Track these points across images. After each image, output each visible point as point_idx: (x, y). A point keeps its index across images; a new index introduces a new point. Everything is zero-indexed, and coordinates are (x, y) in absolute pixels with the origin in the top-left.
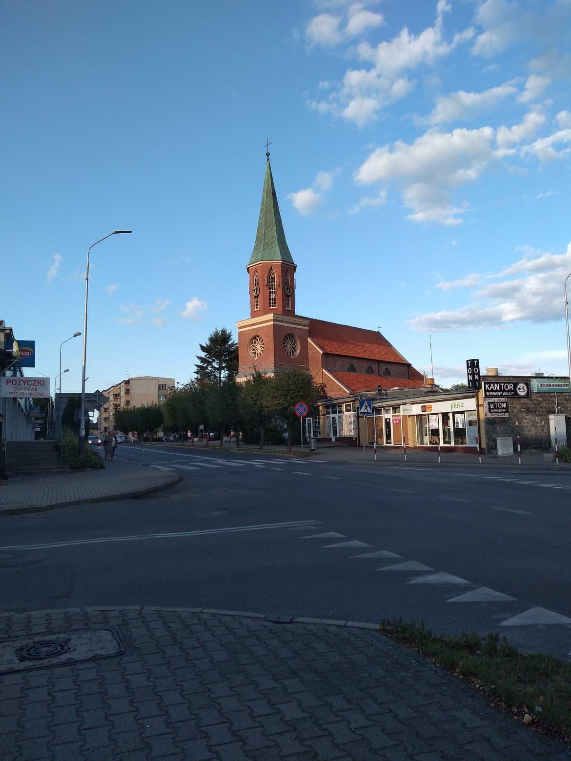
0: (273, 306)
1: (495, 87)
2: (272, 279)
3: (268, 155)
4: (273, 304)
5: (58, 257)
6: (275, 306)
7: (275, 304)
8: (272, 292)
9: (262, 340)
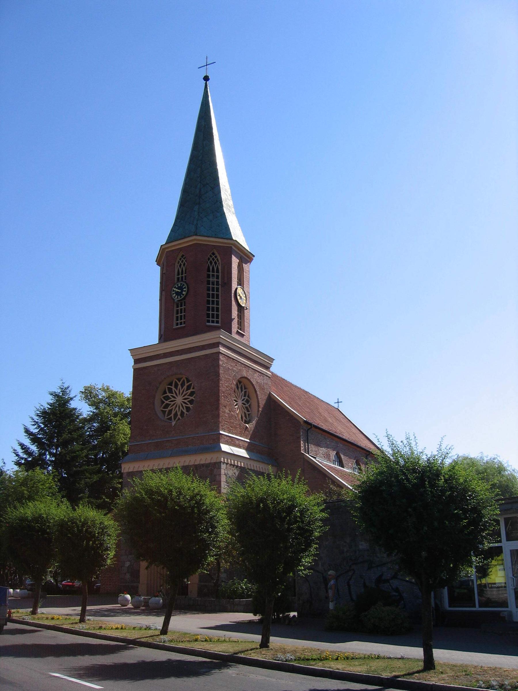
0: (213, 322)
1: (79, 655)
2: (213, 271)
3: (206, 79)
4: (213, 317)
5: (255, 587)
6: (217, 322)
7: (217, 317)
8: (213, 294)
9: (192, 394)
